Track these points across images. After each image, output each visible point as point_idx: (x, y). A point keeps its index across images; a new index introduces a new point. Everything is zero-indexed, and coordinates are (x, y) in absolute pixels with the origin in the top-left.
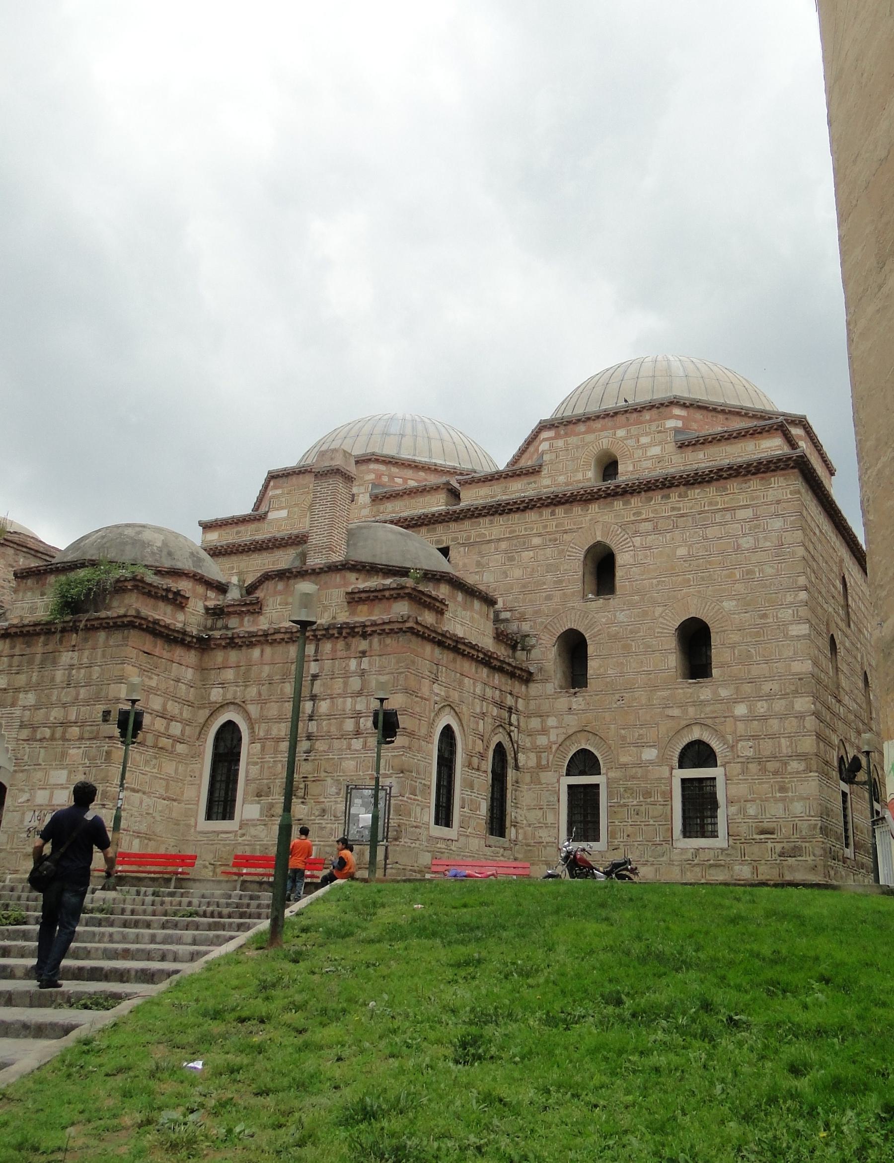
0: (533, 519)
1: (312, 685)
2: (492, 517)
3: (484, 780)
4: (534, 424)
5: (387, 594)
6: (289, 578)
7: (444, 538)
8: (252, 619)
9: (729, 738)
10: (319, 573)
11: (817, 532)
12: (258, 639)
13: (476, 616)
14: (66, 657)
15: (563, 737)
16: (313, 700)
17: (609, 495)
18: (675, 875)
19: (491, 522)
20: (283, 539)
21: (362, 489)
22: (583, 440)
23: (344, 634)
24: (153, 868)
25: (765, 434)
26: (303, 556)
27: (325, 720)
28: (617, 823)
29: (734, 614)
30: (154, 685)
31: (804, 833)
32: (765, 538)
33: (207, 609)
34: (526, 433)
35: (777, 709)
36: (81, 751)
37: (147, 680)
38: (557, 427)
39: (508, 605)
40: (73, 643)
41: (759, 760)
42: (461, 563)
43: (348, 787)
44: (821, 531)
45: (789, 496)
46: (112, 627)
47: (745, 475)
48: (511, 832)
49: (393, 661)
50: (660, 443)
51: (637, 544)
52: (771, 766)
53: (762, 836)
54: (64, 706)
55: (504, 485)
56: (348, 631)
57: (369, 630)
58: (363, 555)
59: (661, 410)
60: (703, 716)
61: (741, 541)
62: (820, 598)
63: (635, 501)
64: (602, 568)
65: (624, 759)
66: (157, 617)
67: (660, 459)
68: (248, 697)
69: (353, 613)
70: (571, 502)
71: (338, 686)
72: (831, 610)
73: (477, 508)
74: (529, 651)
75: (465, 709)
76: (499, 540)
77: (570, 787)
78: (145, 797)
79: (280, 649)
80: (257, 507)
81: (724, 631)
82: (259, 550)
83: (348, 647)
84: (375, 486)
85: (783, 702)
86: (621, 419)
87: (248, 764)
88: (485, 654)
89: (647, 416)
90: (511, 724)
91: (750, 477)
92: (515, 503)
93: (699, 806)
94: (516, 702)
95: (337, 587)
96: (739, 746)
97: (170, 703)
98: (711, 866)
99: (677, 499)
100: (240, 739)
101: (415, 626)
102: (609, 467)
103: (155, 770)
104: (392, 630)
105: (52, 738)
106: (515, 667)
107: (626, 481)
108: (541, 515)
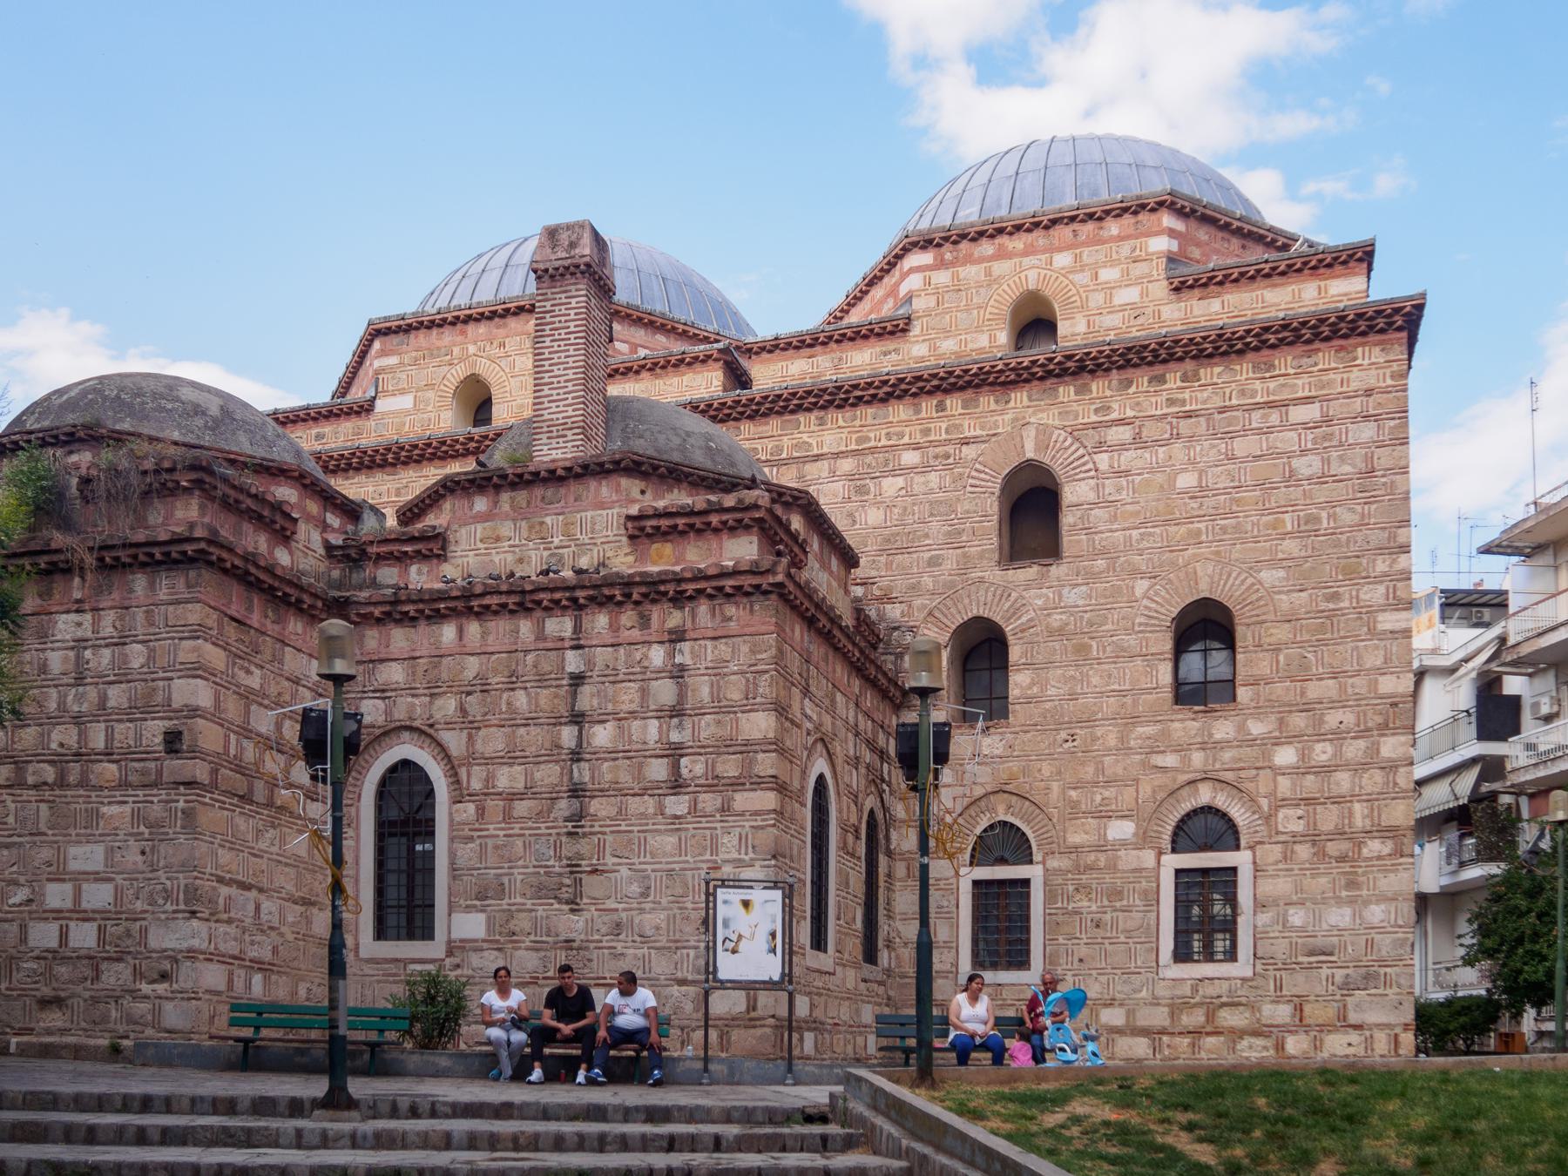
0: (903, 416)
1: (574, 695)
2: (822, 413)
5: (714, 519)
6: (498, 488)
8: (425, 569)
9: (1264, 803)
10: (562, 479)
12: (451, 604)
14: (66, 626)
16: (577, 723)
19: (941, 407)
20: (416, 446)
22: (988, 273)
23: (635, 596)
25: (1338, 268)
27: (606, 760)
28: (1061, 941)
29: (1280, 593)
30: (257, 687)
31: (1384, 953)
32: (1342, 459)
33: (329, 547)
35: (1350, 755)
36: (127, 808)
37: (242, 674)
38: (939, 245)
40: (77, 595)
41: (1314, 838)
43: (707, 883)
45: (1389, 382)
46: (159, 563)
47: (1309, 342)
48: (884, 957)
49: (745, 649)
50: (1138, 282)
52: (1333, 848)
54: (78, 720)
55: (838, 354)
56: (644, 589)
57: (690, 587)
59: (1140, 217)
60: (1218, 766)
61: (1295, 463)
63: (1098, 387)
64: (1032, 512)
65: (1075, 838)
67: (1136, 311)
68: (438, 716)
70: (978, 386)
71: (628, 696)
73: (794, 394)
76: (838, 455)
77: (976, 883)
78: (262, 897)
79: (500, 627)
81: (1264, 622)
82: (369, 468)
83: (645, 622)
85: (1362, 743)
86: (1063, 233)
87: (452, 840)
89: (1113, 227)
90: (883, 780)
91: (1317, 345)
92: (870, 384)
93: (1205, 916)
95: (602, 506)
96: (1280, 815)
98: (1224, 1005)
99: (1179, 384)
100: (430, 793)
102: (1035, 322)
103: (275, 849)
104: (738, 588)
105: (61, 782)
108: (918, 412)
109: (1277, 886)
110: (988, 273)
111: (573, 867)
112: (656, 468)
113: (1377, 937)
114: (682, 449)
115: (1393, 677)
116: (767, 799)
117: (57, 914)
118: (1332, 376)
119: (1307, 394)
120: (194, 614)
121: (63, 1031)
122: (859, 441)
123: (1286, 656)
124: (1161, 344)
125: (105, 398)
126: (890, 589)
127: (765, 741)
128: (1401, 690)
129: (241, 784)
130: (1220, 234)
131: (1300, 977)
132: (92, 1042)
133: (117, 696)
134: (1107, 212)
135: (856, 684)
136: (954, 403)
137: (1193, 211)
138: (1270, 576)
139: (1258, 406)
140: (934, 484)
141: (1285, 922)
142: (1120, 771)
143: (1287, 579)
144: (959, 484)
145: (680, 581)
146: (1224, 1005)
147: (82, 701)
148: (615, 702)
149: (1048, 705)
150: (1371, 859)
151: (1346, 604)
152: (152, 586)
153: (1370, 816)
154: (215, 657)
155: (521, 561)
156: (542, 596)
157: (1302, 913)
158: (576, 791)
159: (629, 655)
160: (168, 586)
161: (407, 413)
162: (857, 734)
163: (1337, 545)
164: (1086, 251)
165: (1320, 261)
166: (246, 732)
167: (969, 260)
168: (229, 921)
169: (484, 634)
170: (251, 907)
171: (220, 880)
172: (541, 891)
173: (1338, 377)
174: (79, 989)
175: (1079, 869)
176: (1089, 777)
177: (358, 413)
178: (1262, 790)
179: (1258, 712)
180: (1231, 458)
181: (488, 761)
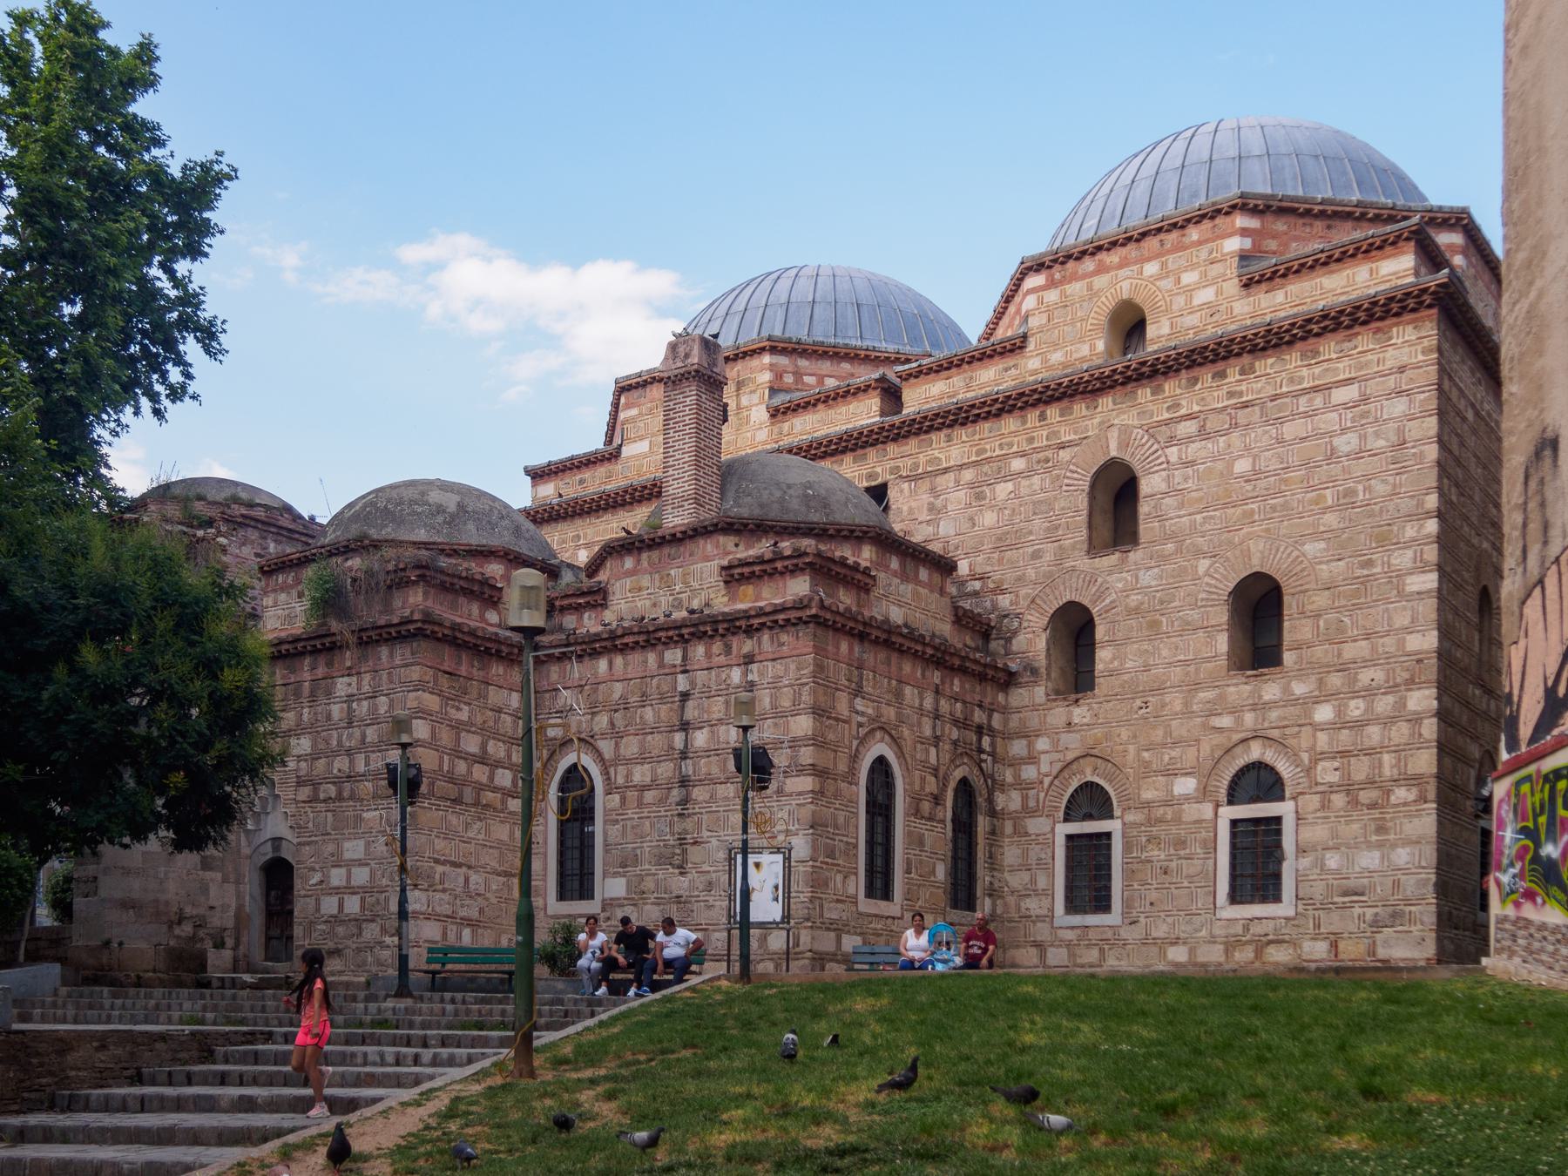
0: (1013, 428)
1: (683, 708)
3: (939, 836)
4: (1012, 267)
5: (779, 565)
6: (640, 550)
7: (879, 470)
9: (1305, 757)
10: (681, 540)
11: (1470, 415)
13: (923, 591)
14: (342, 686)
15: (1058, 766)
17: (1128, 380)
18: (1212, 955)
19: (949, 439)
21: (755, 398)
22: (1090, 288)
24: (493, 967)
25: (1388, 249)
26: (658, 514)
32: (1377, 435)
34: (1002, 284)
35: (1379, 710)
37: (453, 711)
38: (1050, 267)
39: (979, 570)
40: (348, 664)
41: (1348, 788)
42: (905, 508)
44: (1477, 414)
45: (1421, 357)
47: (1349, 327)
49: (793, 667)
51: (1173, 459)
52: (1365, 796)
53: (1346, 899)
54: (349, 753)
57: (756, 621)
58: (743, 509)
59: (1217, 221)
61: (1336, 441)
62: (1466, 528)
63: (1170, 387)
64: (1117, 501)
65: (1148, 795)
66: (459, 620)
67: (1211, 309)
69: (733, 599)
70: (1071, 396)
72: (1485, 545)
74: (1009, 640)
75: (906, 732)
76: (961, 467)
77: (1070, 838)
78: (471, 872)
79: (635, 657)
80: (609, 439)
83: (728, 650)
84: (773, 391)
85: (1390, 699)
86: (1152, 243)
87: (605, 822)
88: (936, 648)
89: (1194, 233)
90: (981, 751)
91: (1357, 329)
92: (984, 403)
93: (1257, 864)
94: (990, 717)
95: (707, 559)
96: (1319, 768)
97: (491, 743)
98: (1270, 942)
99: (1238, 377)
101: (821, 613)
102: (1130, 325)
103: (481, 836)
105: (340, 798)
106: (985, 666)
107: (1155, 352)
108: (1025, 422)
109: (1316, 833)
110: (1090, 288)
111: (682, 840)
112: (826, 530)
113: (1403, 878)
114: (781, 501)
115: (1419, 635)
116: (806, 783)
117: (337, 890)
118: (1369, 357)
119: (1347, 376)
120: (415, 673)
121: (341, 973)
122: (978, 453)
123: (1326, 621)
124: (1219, 344)
125: (377, 509)
126: (1001, 581)
127: (806, 738)
128: (1426, 646)
129: (453, 791)
130: (1301, 221)
131: (1335, 916)
132: (356, 979)
133: (371, 734)
134: (1188, 220)
135: (936, 676)
136: (1053, 412)
137: (1268, 207)
138: (1312, 548)
139: (1305, 391)
140: (1036, 487)
141: (1323, 865)
142: (1184, 733)
143: (1327, 550)
144: (1057, 484)
145: (749, 617)
146: (1270, 942)
147: (351, 739)
148: (709, 713)
149: (1126, 677)
150: (1397, 805)
151: (1378, 570)
152: (391, 655)
153: (1397, 765)
154: (432, 702)
155: (655, 605)
156: (661, 634)
157: (1337, 857)
158: (684, 782)
159: (718, 676)
160: (402, 653)
161: (645, 456)
162: (937, 716)
163: (1371, 515)
164: (1171, 258)
165: (1371, 245)
166: (457, 753)
167: (1074, 278)
168: (444, 891)
169: (626, 665)
170: (461, 880)
171: (437, 861)
172: (662, 859)
173: (1375, 357)
174: (349, 942)
175: (1150, 822)
176: (1159, 739)
177: (609, 459)
178: (1304, 745)
179: (1301, 674)
180: (1280, 441)
181: (628, 761)
